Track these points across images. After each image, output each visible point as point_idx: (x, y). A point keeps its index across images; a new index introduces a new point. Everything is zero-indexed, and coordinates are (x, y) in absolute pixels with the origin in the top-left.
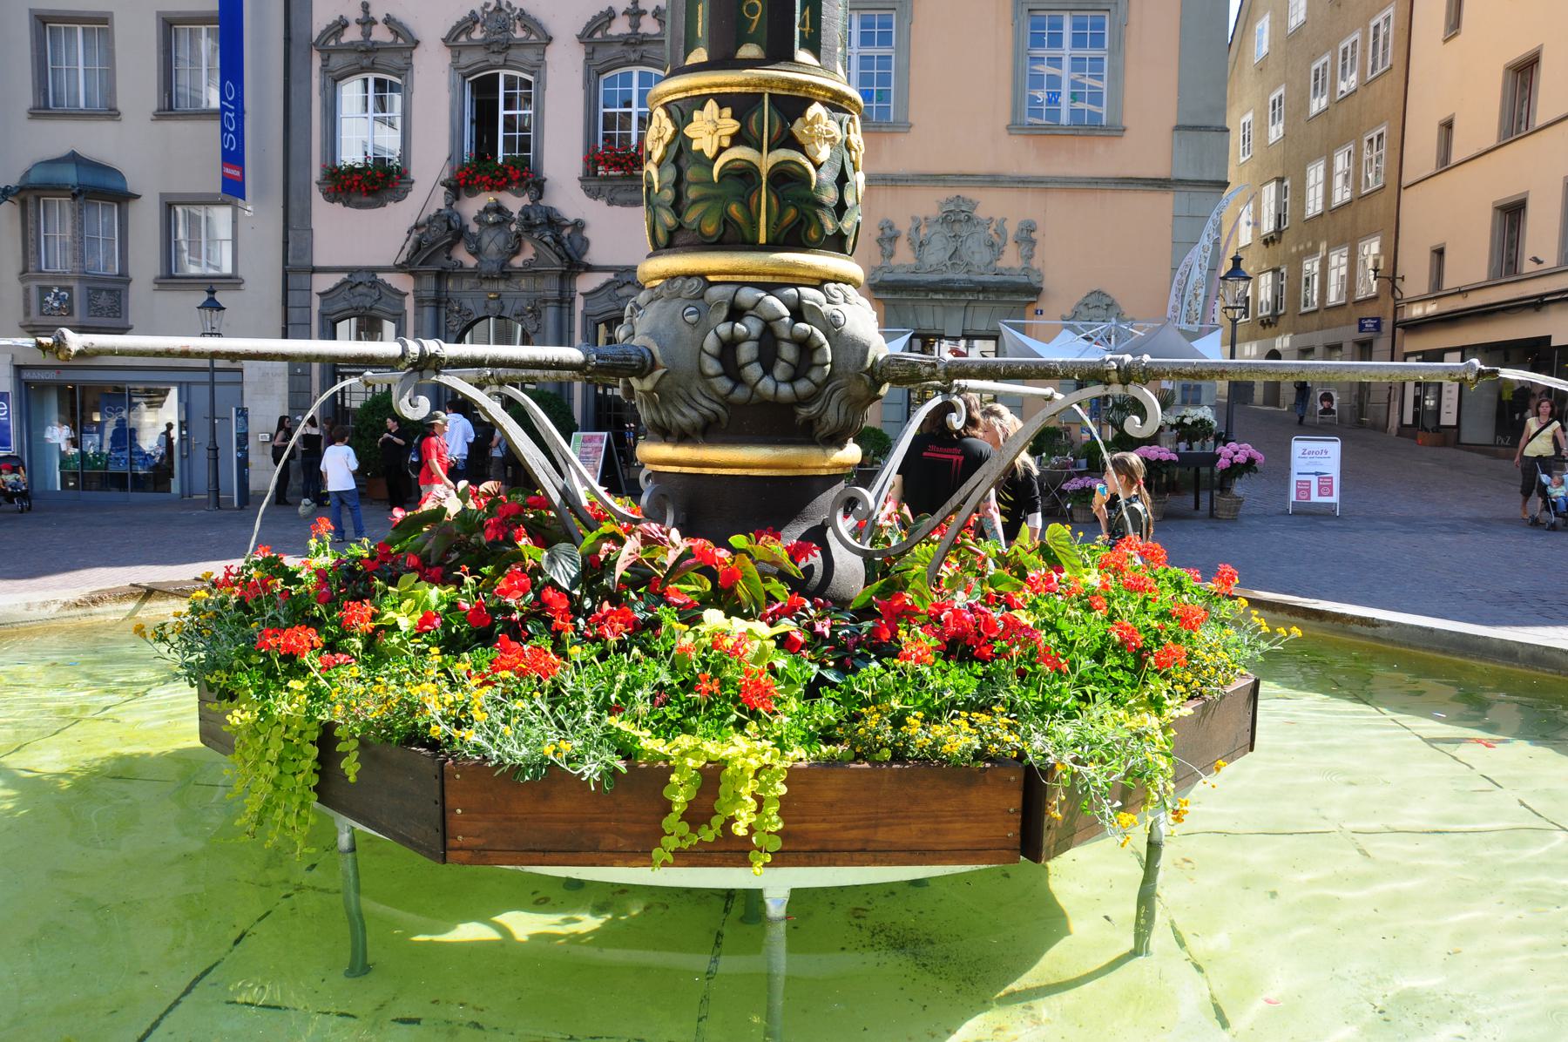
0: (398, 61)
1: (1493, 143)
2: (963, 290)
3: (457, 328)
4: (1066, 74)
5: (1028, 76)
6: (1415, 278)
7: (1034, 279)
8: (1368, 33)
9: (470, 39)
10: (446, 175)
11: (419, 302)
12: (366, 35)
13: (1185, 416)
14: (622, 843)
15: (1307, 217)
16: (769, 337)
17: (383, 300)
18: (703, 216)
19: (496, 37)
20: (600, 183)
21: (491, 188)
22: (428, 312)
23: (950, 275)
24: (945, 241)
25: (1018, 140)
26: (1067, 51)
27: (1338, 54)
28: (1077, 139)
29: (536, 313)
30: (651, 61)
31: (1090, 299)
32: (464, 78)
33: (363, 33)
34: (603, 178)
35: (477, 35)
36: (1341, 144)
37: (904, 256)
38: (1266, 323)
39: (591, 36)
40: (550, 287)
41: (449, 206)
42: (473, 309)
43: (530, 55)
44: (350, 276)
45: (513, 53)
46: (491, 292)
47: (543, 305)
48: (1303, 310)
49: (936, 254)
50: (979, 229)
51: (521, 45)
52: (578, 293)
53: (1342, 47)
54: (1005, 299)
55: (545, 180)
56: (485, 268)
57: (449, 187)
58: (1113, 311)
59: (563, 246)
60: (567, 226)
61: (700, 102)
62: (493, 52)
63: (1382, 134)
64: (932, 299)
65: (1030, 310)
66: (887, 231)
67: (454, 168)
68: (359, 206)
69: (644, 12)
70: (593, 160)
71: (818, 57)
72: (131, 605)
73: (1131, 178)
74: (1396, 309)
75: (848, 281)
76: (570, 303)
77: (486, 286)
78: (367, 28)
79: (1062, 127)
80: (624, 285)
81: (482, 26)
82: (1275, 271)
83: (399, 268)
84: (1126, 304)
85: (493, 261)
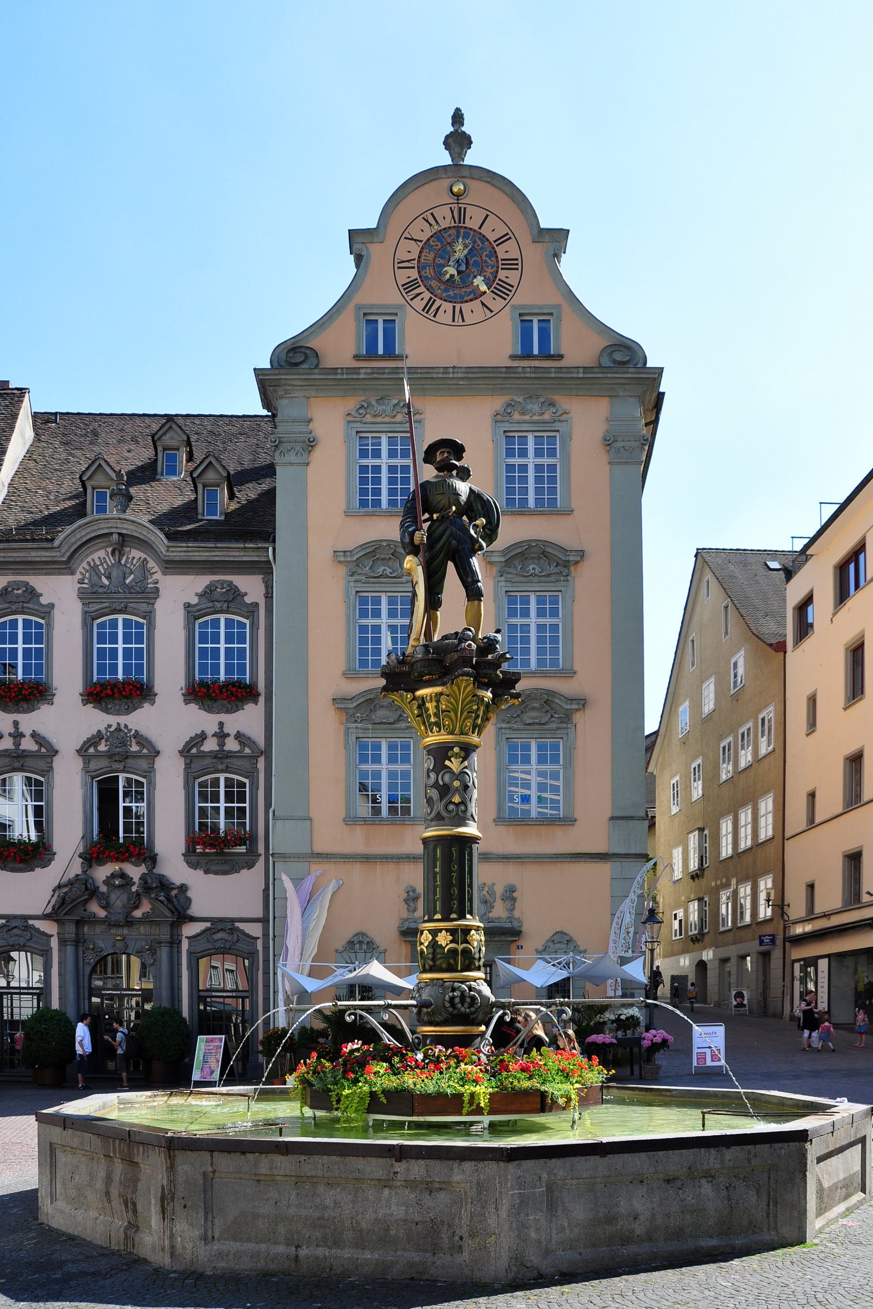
0: (42, 764)
1: (840, 810)
3: (92, 961)
5: (507, 796)
6: (797, 908)
7: (516, 924)
8: (757, 723)
9: (97, 751)
10: (81, 850)
11: (62, 942)
12: (17, 744)
13: (621, 1014)
14: (453, 1110)
15: (721, 859)
17: (33, 939)
18: (441, 963)
19: (117, 750)
20: (199, 858)
21: (117, 859)
22: (70, 949)
25: (502, 829)
26: (534, 765)
27: (738, 736)
29: (153, 951)
30: (233, 770)
31: (555, 937)
32: (93, 778)
33: (14, 744)
34: (201, 854)
35: (102, 747)
36: (743, 804)
38: (695, 940)
39: (189, 751)
40: (164, 933)
41: (84, 872)
43: (143, 764)
44: (7, 922)
45: (130, 762)
46: (118, 936)
48: (722, 929)
51: (137, 756)
52: (184, 937)
53: (741, 731)
54: (496, 939)
55: (157, 855)
56: (113, 918)
57: (85, 859)
58: (571, 946)
59: (173, 902)
60: (175, 888)
61: (440, 931)
62: (115, 761)
65: (513, 947)
66: (411, 894)
67: (86, 846)
68: (13, 870)
69: (228, 735)
70: (192, 842)
71: (472, 916)
72: (166, 1098)
73: (582, 854)
74: (785, 928)
75: (479, 979)
77: (113, 931)
78: (18, 739)
79: (532, 819)
80: (218, 931)
81: (106, 741)
82: (700, 900)
83: (45, 917)
85: (120, 913)
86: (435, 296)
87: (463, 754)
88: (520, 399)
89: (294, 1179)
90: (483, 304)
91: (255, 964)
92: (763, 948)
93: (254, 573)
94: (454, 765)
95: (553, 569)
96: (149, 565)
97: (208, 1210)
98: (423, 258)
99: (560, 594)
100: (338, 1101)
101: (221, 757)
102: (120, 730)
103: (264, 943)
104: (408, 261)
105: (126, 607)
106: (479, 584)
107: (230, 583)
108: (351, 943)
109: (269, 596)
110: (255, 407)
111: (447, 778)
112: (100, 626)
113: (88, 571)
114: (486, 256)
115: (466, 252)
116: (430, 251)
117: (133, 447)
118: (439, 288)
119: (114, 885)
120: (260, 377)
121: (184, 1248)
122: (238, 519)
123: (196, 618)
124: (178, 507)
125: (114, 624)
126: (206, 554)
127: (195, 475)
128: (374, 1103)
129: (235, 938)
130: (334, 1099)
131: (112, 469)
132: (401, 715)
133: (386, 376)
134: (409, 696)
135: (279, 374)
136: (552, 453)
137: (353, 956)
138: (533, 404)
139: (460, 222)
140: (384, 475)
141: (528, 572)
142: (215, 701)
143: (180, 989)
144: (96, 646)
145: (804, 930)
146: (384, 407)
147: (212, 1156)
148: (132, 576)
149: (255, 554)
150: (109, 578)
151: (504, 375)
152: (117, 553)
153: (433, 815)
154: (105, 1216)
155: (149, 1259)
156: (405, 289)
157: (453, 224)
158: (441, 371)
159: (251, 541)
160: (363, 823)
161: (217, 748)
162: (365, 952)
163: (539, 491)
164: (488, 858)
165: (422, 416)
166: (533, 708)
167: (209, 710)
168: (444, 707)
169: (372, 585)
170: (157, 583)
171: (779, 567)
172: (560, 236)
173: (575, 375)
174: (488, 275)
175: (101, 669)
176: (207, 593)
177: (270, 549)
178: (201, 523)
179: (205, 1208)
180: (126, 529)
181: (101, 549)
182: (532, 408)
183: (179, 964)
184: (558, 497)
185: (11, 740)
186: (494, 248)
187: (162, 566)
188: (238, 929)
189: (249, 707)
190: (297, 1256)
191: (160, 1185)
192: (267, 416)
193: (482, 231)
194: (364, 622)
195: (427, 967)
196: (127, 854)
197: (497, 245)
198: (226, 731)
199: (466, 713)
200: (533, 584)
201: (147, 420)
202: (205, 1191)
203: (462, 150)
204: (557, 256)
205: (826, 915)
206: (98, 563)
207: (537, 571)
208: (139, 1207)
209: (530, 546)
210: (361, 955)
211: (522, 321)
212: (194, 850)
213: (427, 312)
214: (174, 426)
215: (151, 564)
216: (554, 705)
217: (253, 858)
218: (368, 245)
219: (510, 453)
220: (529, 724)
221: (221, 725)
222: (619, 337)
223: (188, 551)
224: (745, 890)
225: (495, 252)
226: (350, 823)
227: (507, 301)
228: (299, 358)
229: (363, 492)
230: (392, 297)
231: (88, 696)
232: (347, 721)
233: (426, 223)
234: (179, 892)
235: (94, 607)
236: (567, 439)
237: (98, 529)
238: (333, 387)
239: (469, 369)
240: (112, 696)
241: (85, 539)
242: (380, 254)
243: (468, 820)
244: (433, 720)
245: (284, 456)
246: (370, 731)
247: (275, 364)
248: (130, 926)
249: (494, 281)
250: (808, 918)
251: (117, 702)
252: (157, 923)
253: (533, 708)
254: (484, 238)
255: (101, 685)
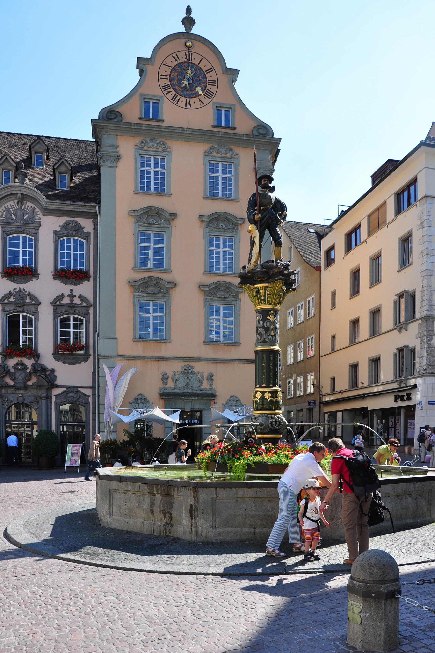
1: (348, 344)
2: (191, 396)
3: (6, 407)
4: (221, 324)
6: (326, 388)
7: (213, 392)
8: (306, 302)
16: (276, 421)
18: (266, 406)
19: (19, 301)
23: (186, 391)
24: (184, 379)
25: (207, 347)
26: (221, 317)
28: (225, 346)
31: (231, 399)
32: (7, 315)
35: (12, 300)
37: (170, 384)
39: (55, 303)
40: (44, 393)
41: (3, 362)
42: (13, 401)
46: (20, 394)
47: (40, 399)
48: (288, 397)
49: (181, 384)
50: (195, 375)
51: (29, 304)
52: (53, 395)
54: (205, 398)
56: (18, 385)
59: (48, 378)
60: (48, 371)
61: (266, 392)
63: (313, 338)
64: (181, 399)
65: (212, 402)
66: (165, 376)
67: (4, 349)
69: (75, 296)
70: (57, 348)
72: (124, 470)
74: (320, 398)
76: (50, 398)
77: (17, 392)
81: (14, 297)
84: (243, 401)
85: (21, 383)
86: (178, 93)
87: (274, 314)
88: (216, 146)
89: (253, 499)
90: (200, 100)
91: (88, 409)
92: (309, 407)
93: (88, 218)
94: (271, 318)
95: (230, 226)
96: (36, 210)
97: (214, 514)
98: (172, 75)
99: (233, 238)
100: (231, 468)
101: (72, 306)
102: (21, 291)
103: (92, 398)
104: (165, 76)
105: (24, 230)
106: (281, 240)
107: (77, 222)
108: (136, 399)
109: (95, 229)
110: (88, 136)
111: (268, 324)
112: (62, 242)
113: (4, 211)
114: (202, 77)
115: (192, 74)
116: (175, 72)
117: (17, 150)
118: (179, 90)
119: (18, 369)
120: (94, 123)
121: (202, 531)
122: (76, 190)
123: (59, 238)
124: (45, 182)
125: (17, 238)
126: (66, 207)
127: (55, 167)
128: (249, 468)
129: (79, 395)
130: (229, 467)
131: (13, 160)
132: (160, 290)
133: (155, 129)
134: (252, 287)
135: (104, 123)
136: (230, 172)
137: (137, 405)
138: (223, 149)
139: (189, 60)
140: (152, 176)
141: (219, 227)
142: (69, 279)
143: (51, 421)
144: (8, 249)
145: (330, 399)
146: (153, 144)
147: (216, 490)
148: (27, 215)
149: (89, 208)
150: (15, 215)
151: (210, 134)
152: (20, 203)
153: (261, 340)
154: (148, 521)
155: (181, 538)
156: (163, 89)
157: (186, 61)
158: (181, 129)
159: (88, 202)
160: (142, 341)
161: (70, 302)
162: (143, 404)
163: (224, 189)
164: (201, 360)
165: (171, 149)
166: (221, 290)
167: (66, 283)
168: (269, 293)
169: (146, 227)
170: (40, 219)
171: (314, 231)
172: (236, 72)
173: (242, 138)
174: (202, 86)
175: (11, 260)
176: (65, 226)
177: (97, 207)
178: (59, 191)
179: (212, 514)
180: (25, 192)
181: (12, 200)
182: (222, 151)
183: (51, 409)
184: (233, 193)
185: (68, 298)
186: (205, 74)
187: (43, 211)
188: (80, 392)
189: (86, 283)
190: (255, 532)
191: (189, 504)
192: (93, 141)
193: (199, 65)
194: (142, 245)
195: (259, 408)
196: (25, 353)
197: (207, 73)
198: (74, 294)
199: (277, 296)
200: (222, 233)
201: (22, 137)
202: (212, 506)
203: (191, 26)
204: (234, 81)
205: (341, 392)
206: (10, 207)
207: (223, 227)
208: (174, 515)
209: (220, 215)
210: (141, 405)
211: (217, 110)
212: (58, 352)
213: (174, 101)
214: (41, 142)
215: (37, 210)
216: (231, 290)
217: (87, 357)
218: (146, 66)
219: (211, 171)
220: (220, 298)
221: (72, 291)
222: (261, 122)
223: (56, 205)
224: (300, 380)
225: (206, 76)
226: (135, 341)
227: (211, 100)
228: (113, 116)
229: (143, 183)
230: (157, 92)
231: (4, 273)
232: (135, 292)
233: (173, 59)
234: (50, 373)
235: (8, 229)
236: (237, 167)
237: (11, 191)
238: (129, 132)
239: (194, 130)
240: (17, 274)
241: (4, 195)
242: (150, 69)
243: (276, 343)
244: (262, 298)
245: (105, 162)
246: (145, 297)
247: (101, 118)
248: (26, 389)
249: (205, 90)
250: (332, 393)
251: (19, 277)
252: (40, 388)
253: (221, 290)
254: (200, 69)
255: (12, 268)
